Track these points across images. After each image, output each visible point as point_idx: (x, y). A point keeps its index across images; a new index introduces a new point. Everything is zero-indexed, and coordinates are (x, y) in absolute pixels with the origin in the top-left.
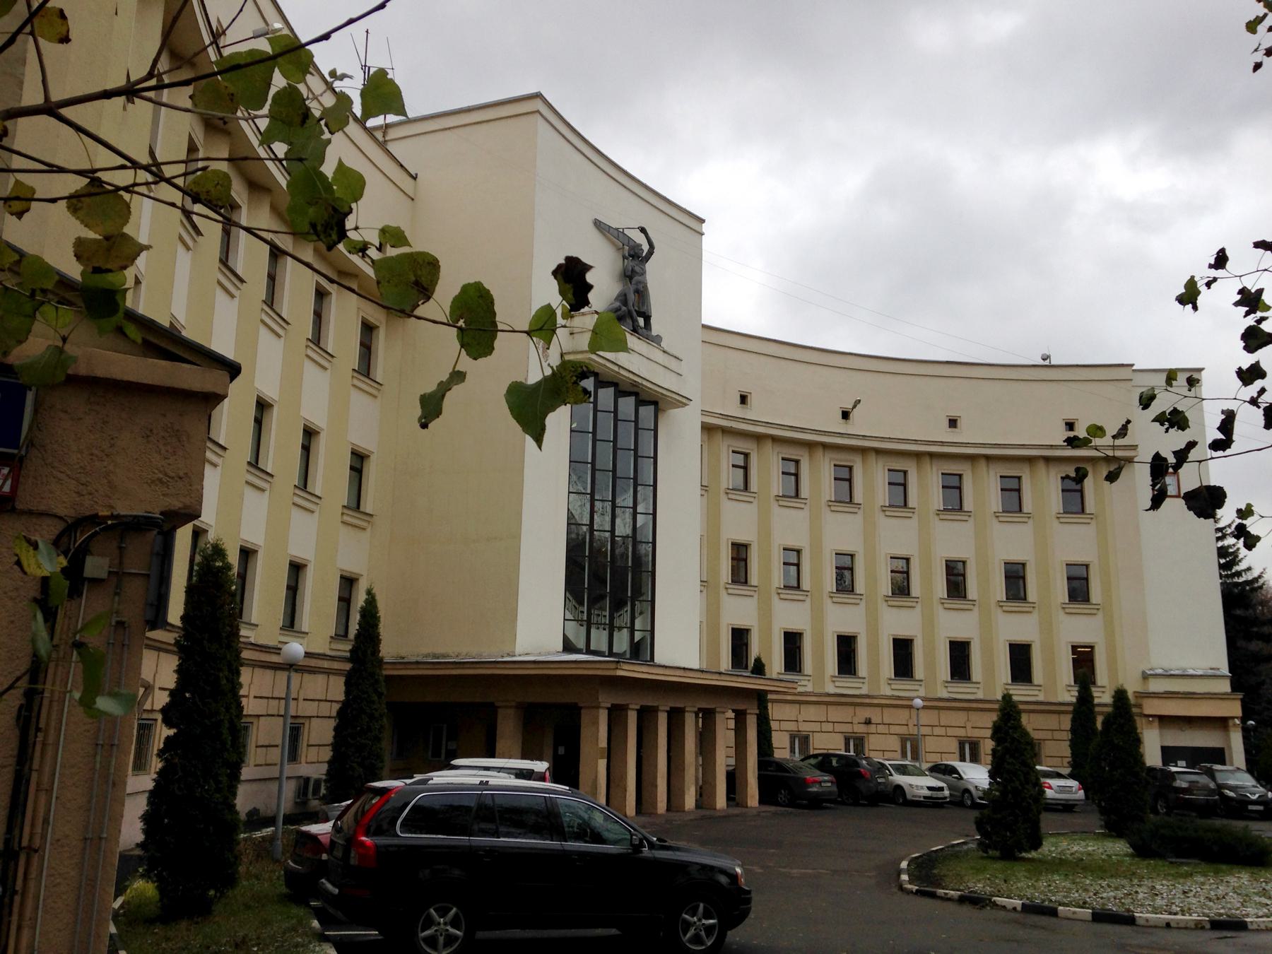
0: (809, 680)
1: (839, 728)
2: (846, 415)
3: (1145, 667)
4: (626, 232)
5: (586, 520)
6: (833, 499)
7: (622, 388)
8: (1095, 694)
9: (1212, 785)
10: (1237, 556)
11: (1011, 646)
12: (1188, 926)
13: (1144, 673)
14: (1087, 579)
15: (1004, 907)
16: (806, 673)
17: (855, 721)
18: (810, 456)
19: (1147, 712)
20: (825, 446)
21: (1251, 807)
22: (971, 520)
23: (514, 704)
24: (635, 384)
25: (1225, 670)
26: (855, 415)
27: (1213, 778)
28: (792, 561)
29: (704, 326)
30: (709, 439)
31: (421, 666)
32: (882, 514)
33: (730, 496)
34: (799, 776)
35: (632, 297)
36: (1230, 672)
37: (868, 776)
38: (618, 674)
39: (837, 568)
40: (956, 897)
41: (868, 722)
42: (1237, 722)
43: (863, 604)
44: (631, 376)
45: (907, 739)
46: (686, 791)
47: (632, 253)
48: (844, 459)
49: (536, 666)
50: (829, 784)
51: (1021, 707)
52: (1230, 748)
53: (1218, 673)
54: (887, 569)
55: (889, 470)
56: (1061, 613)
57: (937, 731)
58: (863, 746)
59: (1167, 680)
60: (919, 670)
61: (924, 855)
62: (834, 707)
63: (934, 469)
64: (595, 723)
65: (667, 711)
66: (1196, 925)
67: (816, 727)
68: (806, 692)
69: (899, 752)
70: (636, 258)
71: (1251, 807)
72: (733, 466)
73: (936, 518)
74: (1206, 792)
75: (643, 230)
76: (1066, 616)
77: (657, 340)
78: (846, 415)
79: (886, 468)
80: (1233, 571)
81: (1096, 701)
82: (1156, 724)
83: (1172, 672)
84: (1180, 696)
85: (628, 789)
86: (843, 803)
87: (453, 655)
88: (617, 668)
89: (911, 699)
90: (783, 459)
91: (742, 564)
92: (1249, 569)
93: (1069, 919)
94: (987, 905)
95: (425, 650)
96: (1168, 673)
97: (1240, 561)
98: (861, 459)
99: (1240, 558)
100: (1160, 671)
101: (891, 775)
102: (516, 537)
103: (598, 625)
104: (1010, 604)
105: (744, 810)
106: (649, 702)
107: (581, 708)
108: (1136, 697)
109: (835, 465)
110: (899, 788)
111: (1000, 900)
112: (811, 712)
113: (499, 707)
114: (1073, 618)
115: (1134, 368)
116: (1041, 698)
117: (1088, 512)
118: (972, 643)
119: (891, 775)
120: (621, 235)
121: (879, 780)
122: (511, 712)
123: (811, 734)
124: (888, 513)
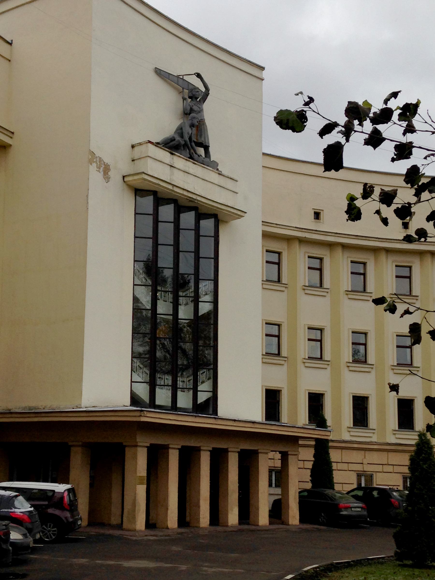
4: (185, 78)
5: (149, 306)
6: (307, 285)
7: (182, 203)
11: (354, 397)
16: (371, 428)
17: (365, 462)
23: (80, 443)
24: (191, 200)
28: (361, 342)
29: (264, 154)
30: (288, 247)
31: (13, 415)
32: (346, 296)
33: (307, 292)
34: (336, 503)
35: (188, 130)
37: (396, 504)
38: (142, 420)
44: (185, 193)
45: (273, 470)
46: (230, 511)
47: (191, 95)
48: (360, 257)
49: (88, 414)
50: (359, 509)
51: (331, 444)
61: (353, 561)
64: (135, 457)
65: (210, 451)
67: (379, 468)
68: (371, 442)
70: (194, 99)
72: (309, 268)
73: (346, 296)
75: (199, 76)
76: (305, 368)
77: (214, 166)
79: (349, 260)
85: (169, 508)
86: (372, 524)
87: (41, 407)
88: (141, 416)
90: (352, 262)
91: (362, 348)
95: (23, 405)
98: (419, 262)
102: (81, 318)
103: (183, 389)
105: (288, 527)
106: (192, 443)
107: (126, 446)
109: (396, 266)
112: (374, 457)
113: (126, 446)
118: (370, 398)
120: (181, 81)
122: (79, 449)
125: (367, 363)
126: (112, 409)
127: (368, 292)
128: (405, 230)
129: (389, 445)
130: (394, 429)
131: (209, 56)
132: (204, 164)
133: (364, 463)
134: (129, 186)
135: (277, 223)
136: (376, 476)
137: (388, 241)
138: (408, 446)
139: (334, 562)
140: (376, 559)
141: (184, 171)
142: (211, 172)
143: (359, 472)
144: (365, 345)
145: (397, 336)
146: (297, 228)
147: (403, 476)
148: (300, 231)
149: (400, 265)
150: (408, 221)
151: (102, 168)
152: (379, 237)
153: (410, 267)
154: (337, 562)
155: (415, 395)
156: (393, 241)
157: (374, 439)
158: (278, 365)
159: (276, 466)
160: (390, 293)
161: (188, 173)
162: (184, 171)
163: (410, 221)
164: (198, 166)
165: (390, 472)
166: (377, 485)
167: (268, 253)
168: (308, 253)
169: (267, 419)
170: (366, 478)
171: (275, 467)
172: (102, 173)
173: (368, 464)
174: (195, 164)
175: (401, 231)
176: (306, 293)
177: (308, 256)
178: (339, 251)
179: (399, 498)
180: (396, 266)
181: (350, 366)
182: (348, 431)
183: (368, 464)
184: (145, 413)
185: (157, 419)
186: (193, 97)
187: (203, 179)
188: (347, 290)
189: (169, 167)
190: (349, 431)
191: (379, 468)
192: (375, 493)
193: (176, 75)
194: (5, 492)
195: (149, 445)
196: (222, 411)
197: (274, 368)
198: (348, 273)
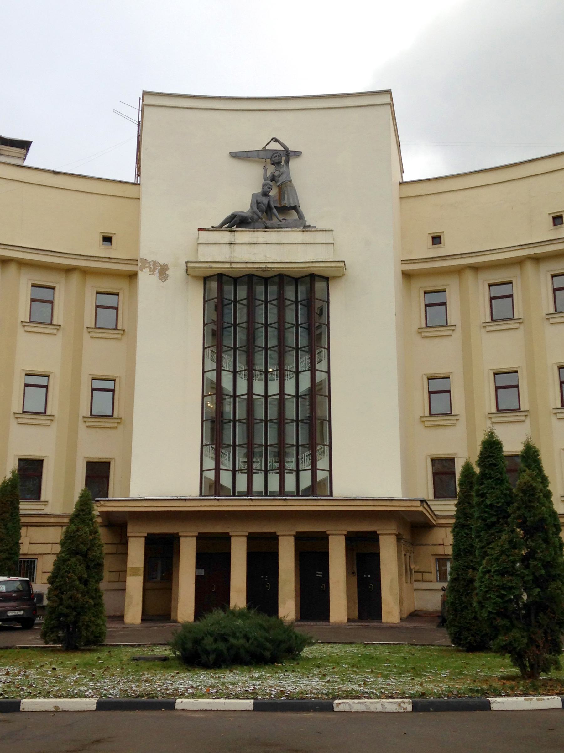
4: (268, 148)
21: (317, 575)
33: (552, 321)
44: (249, 266)
71: (317, 575)
126: (194, 498)
131: (342, 109)
132: (281, 228)
134: (196, 277)
135: (491, 249)
141: (249, 244)
142: (290, 232)
146: (522, 245)
148: (528, 248)
151: (157, 271)
158: (516, 423)
161: (256, 244)
162: (249, 244)
164: (272, 232)
169: (434, 498)
172: (158, 275)
174: (267, 231)
178: (469, 276)
184: (102, 502)
185: (245, 507)
186: (277, 163)
187: (278, 244)
189: (228, 246)
193: (261, 149)
194: (104, 581)
195: (346, 533)
196: (337, 493)
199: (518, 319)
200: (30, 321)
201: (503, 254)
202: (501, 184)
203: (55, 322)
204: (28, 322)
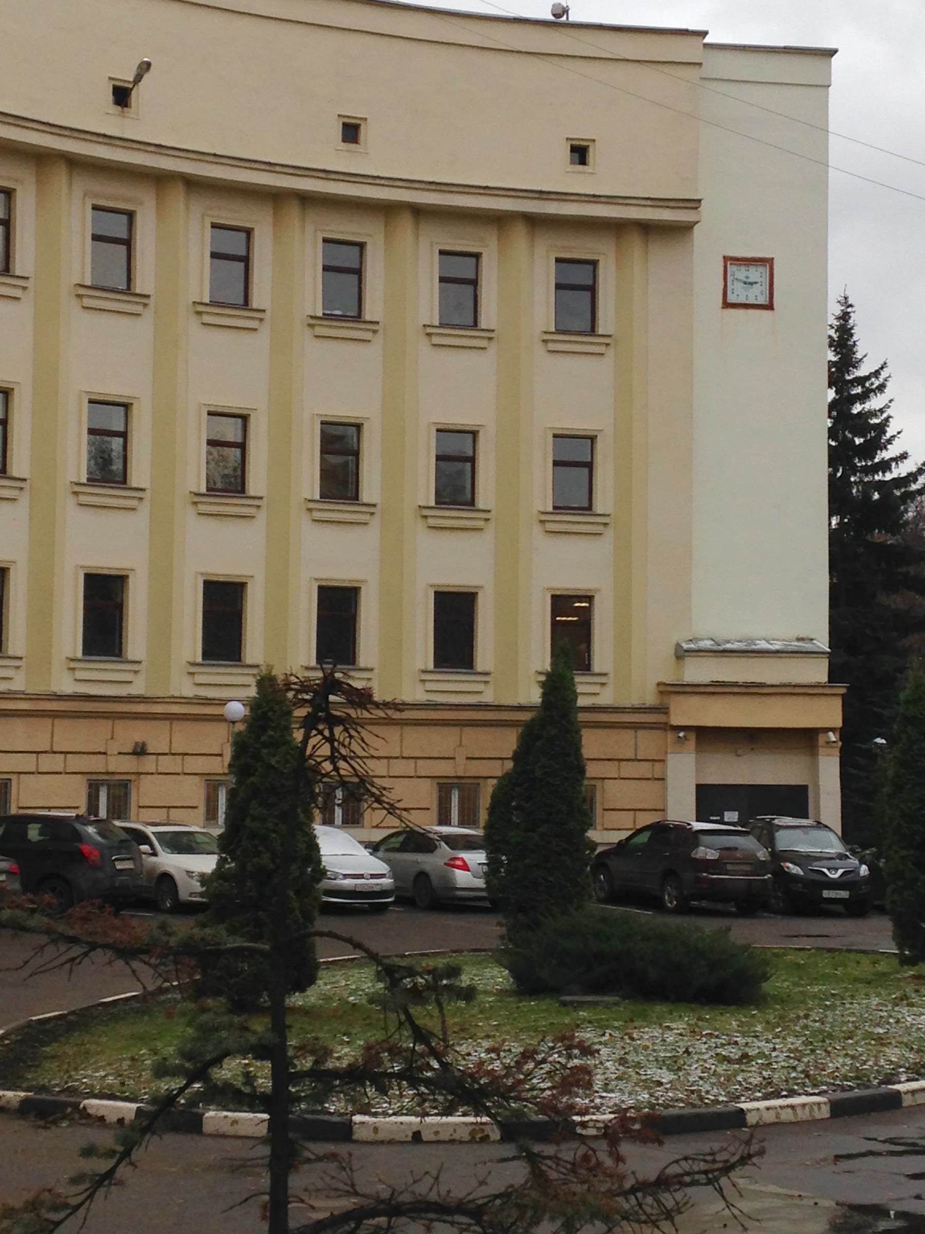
0: (18, 668)
1: (76, 763)
2: (122, 96)
3: (680, 636)
6: (88, 283)
8: (580, 689)
9: (762, 854)
10: (885, 432)
12: (457, 1136)
13: (678, 646)
14: (472, 460)
15: (102, 1119)
17: (114, 748)
18: (276, 224)
19: (676, 721)
20: (74, 163)
21: (826, 894)
22: (378, 340)
25: (823, 643)
26: (140, 96)
27: (769, 840)
28: (115, 429)
36: (830, 648)
37: (95, 857)
39: (91, 431)
40: (15, 1104)
41: (140, 751)
42: (832, 737)
43: (145, 509)
52: (817, 786)
53: (807, 646)
54: (200, 438)
55: (214, 226)
56: (537, 529)
57: (47, 762)
58: (127, 795)
59: (716, 660)
60: (484, 655)
61: (72, 1013)
62: (66, 722)
63: (310, 228)
66: (472, 1133)
67: (27, 763)
68: (10, 692)
69: (202, 809)
71: (826, 894)
73: (308, 332)
74: (747, 868)
78: (122, 96)
80: (876, 460)
81: (581, 702)
82: (692, 742)
83: (729, 646)
84: (736, 690)
89: (223, 702)
91: (117, 443)
92: (904, 456)
93: (224, 1136)
94: (64, 1118)
96: (721, 648)
97: (889, 441)
98: (269, 219)
99: (888, 435)
100: (707, 644)
101: (155, 854)
104: (326, 506)
108: (661, 692)
110: (166, 878)
111: (94, 1105)
114: (562, 541)
115: (708, 40)
116: (488, 697)
117: (601, 332)
118: (131, 580)
119: (155, 854)
121: (119, 866)
123: (14, 777)
124: (207, 319)
125: (8, 474)
127: (17, 274)
128: (119, 108)
129: (59, 700)
130: (71, 655)
133: (108, 753)
136: (19, 783)
137: (76, 134)
138: (98, 701)
139: (34, 1018)
140: (121, 1002)
143: (94, 777)
144: (124, 435)
145: (91, 402)
147: (88, 780)
149: (118, 209)
150: (131, 86)
152: (51, 122)
153: (131, 215)
154: (39, 1020)
155: (362, 578)
156: (88, 137)
157: (19, 683)
159: (110, 771)
160: (76, 283)
163: (136, 87)
165: (30, 773)
166: (22, 808)
167: (216, 230)
168: (96, 196)
170: (112, 791)
171: (108, 773)
173: (120, 753)
175: (111, 112)
176: (204, 322)
177: (212, 223)
179: (99, 839)
180: (95, 208)
181: (80, 492)
182: (70, 669)
183: (120, 753)
188: (81, 283)
190: (73, 669)
191: (27, 763)
192: (33, 833)
197: (230, 525)
198: (83, 235)
199: (371, 322)
200: (556, 330)
201: (387, 189)
202: (433, 46)
203: (368, 317)
204: (553, 333)
